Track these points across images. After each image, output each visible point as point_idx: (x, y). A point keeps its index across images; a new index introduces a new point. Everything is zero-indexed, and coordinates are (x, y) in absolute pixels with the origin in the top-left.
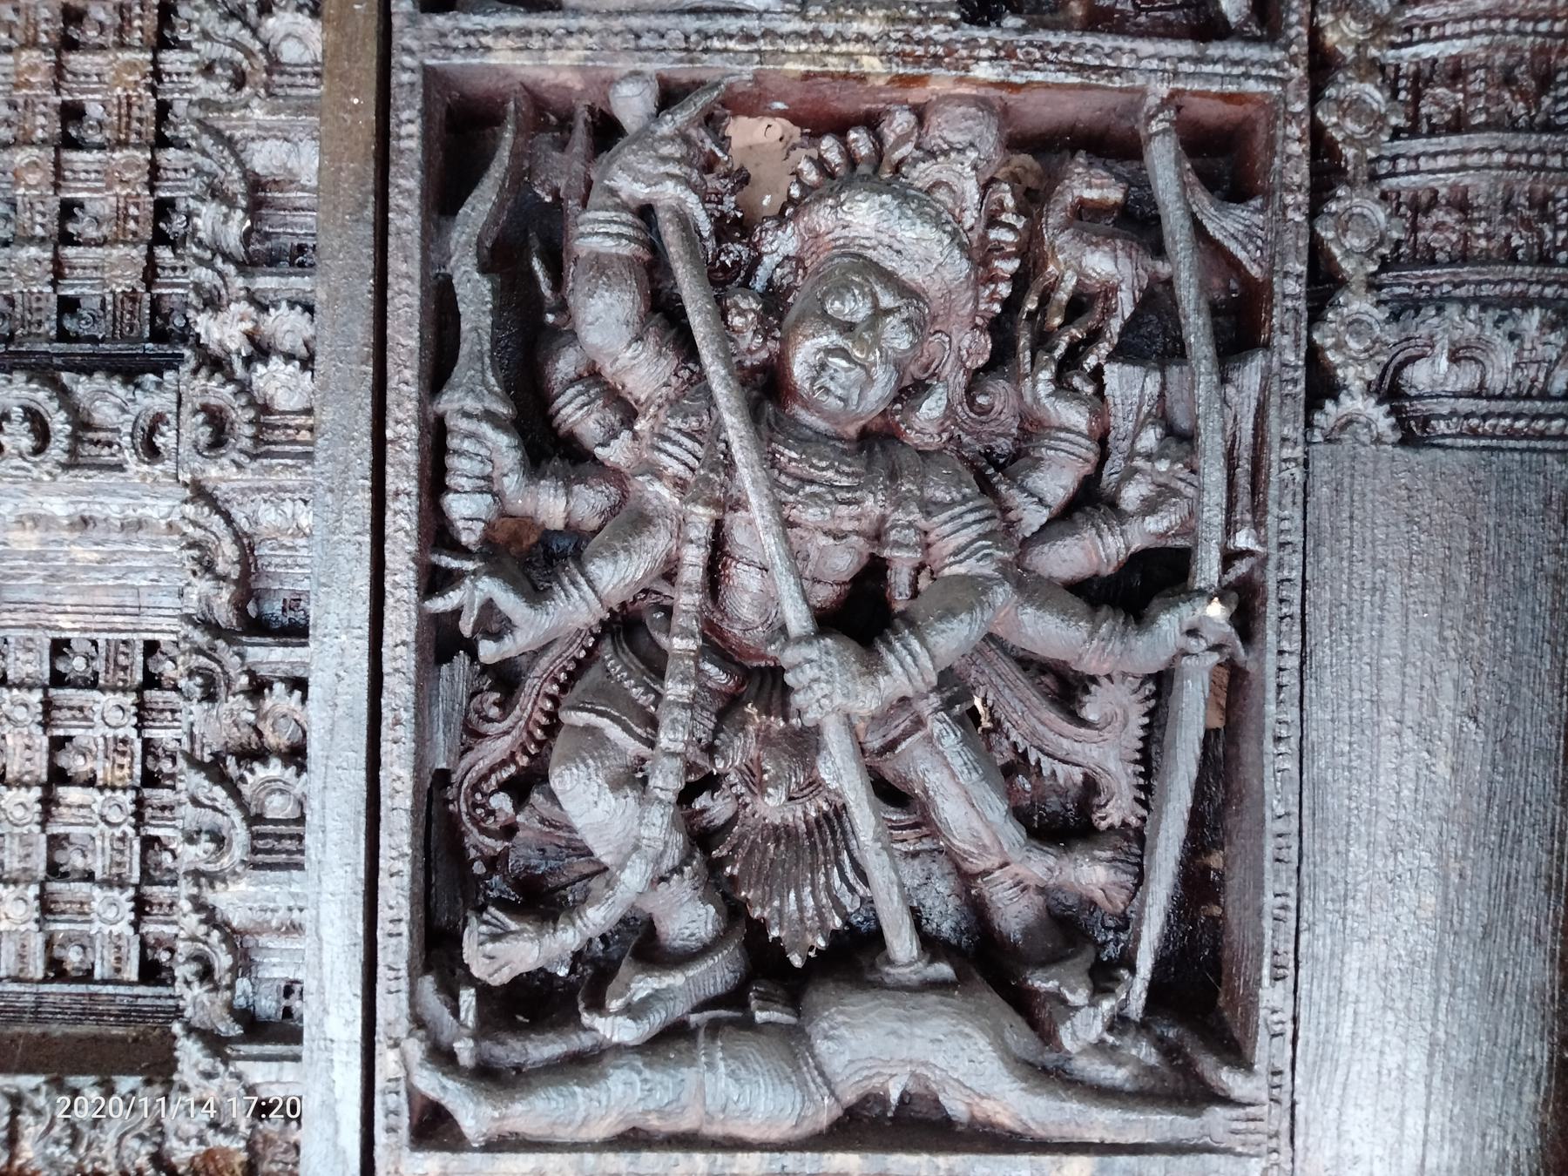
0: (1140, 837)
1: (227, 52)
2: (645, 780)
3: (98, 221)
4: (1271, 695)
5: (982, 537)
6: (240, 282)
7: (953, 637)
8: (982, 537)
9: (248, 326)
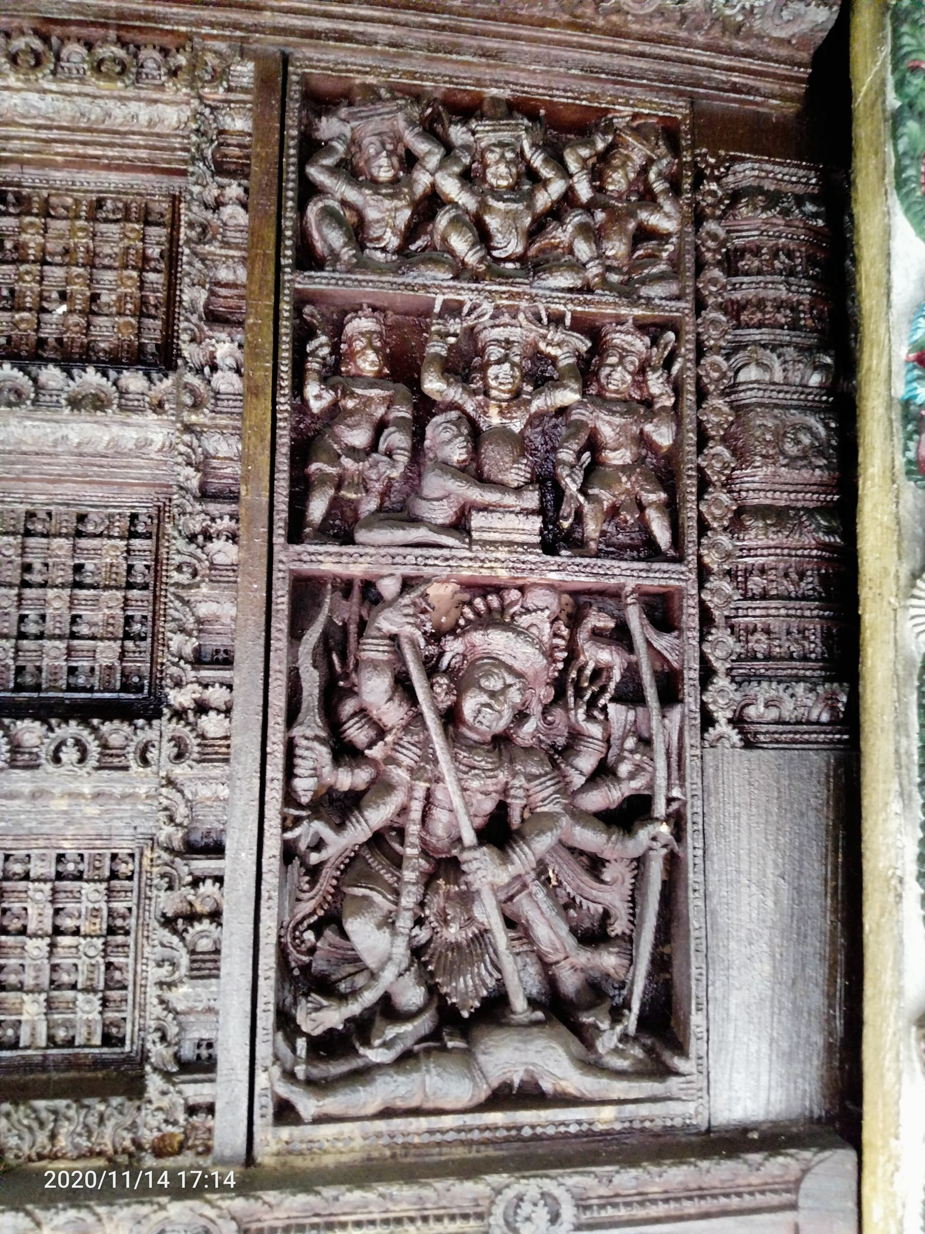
0: (631, 940)
1: (188, 559)
2: (393, 923)
3: (92, 624)
4: (691, 869)
5: (555, 792)
6: (193, 673)
7: (543, 843)
8: (555, 792)
9: (197, 696)
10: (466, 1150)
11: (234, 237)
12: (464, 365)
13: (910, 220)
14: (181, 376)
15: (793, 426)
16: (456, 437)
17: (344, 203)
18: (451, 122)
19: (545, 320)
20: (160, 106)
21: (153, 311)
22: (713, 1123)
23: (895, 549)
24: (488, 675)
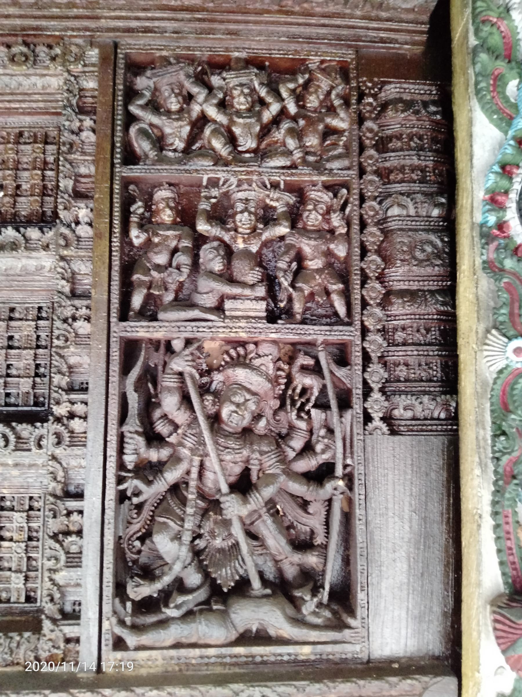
1: (63, 332)
2: (180, 538)
3: (17, 369)
4: (357, 506)
5: (277, 462)
6: (66, 397)
7: (268, 492)
8: (277, 462)
9: (68, 409)
10: (222, 668)
11: (89, 149)
12: (221, 215)
13: (485, 114)
14: (58, 229)
15: (421, 241)
16: (216, 256)
17: (151, 125)
18: (212, 74)
19: (269, 186)
20: (48, 77)
21: (50, 192)
22: (372, 657)
23: (476, 315)
24: (235, 394)
